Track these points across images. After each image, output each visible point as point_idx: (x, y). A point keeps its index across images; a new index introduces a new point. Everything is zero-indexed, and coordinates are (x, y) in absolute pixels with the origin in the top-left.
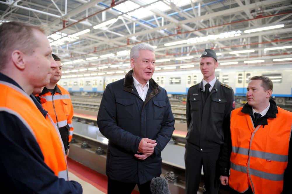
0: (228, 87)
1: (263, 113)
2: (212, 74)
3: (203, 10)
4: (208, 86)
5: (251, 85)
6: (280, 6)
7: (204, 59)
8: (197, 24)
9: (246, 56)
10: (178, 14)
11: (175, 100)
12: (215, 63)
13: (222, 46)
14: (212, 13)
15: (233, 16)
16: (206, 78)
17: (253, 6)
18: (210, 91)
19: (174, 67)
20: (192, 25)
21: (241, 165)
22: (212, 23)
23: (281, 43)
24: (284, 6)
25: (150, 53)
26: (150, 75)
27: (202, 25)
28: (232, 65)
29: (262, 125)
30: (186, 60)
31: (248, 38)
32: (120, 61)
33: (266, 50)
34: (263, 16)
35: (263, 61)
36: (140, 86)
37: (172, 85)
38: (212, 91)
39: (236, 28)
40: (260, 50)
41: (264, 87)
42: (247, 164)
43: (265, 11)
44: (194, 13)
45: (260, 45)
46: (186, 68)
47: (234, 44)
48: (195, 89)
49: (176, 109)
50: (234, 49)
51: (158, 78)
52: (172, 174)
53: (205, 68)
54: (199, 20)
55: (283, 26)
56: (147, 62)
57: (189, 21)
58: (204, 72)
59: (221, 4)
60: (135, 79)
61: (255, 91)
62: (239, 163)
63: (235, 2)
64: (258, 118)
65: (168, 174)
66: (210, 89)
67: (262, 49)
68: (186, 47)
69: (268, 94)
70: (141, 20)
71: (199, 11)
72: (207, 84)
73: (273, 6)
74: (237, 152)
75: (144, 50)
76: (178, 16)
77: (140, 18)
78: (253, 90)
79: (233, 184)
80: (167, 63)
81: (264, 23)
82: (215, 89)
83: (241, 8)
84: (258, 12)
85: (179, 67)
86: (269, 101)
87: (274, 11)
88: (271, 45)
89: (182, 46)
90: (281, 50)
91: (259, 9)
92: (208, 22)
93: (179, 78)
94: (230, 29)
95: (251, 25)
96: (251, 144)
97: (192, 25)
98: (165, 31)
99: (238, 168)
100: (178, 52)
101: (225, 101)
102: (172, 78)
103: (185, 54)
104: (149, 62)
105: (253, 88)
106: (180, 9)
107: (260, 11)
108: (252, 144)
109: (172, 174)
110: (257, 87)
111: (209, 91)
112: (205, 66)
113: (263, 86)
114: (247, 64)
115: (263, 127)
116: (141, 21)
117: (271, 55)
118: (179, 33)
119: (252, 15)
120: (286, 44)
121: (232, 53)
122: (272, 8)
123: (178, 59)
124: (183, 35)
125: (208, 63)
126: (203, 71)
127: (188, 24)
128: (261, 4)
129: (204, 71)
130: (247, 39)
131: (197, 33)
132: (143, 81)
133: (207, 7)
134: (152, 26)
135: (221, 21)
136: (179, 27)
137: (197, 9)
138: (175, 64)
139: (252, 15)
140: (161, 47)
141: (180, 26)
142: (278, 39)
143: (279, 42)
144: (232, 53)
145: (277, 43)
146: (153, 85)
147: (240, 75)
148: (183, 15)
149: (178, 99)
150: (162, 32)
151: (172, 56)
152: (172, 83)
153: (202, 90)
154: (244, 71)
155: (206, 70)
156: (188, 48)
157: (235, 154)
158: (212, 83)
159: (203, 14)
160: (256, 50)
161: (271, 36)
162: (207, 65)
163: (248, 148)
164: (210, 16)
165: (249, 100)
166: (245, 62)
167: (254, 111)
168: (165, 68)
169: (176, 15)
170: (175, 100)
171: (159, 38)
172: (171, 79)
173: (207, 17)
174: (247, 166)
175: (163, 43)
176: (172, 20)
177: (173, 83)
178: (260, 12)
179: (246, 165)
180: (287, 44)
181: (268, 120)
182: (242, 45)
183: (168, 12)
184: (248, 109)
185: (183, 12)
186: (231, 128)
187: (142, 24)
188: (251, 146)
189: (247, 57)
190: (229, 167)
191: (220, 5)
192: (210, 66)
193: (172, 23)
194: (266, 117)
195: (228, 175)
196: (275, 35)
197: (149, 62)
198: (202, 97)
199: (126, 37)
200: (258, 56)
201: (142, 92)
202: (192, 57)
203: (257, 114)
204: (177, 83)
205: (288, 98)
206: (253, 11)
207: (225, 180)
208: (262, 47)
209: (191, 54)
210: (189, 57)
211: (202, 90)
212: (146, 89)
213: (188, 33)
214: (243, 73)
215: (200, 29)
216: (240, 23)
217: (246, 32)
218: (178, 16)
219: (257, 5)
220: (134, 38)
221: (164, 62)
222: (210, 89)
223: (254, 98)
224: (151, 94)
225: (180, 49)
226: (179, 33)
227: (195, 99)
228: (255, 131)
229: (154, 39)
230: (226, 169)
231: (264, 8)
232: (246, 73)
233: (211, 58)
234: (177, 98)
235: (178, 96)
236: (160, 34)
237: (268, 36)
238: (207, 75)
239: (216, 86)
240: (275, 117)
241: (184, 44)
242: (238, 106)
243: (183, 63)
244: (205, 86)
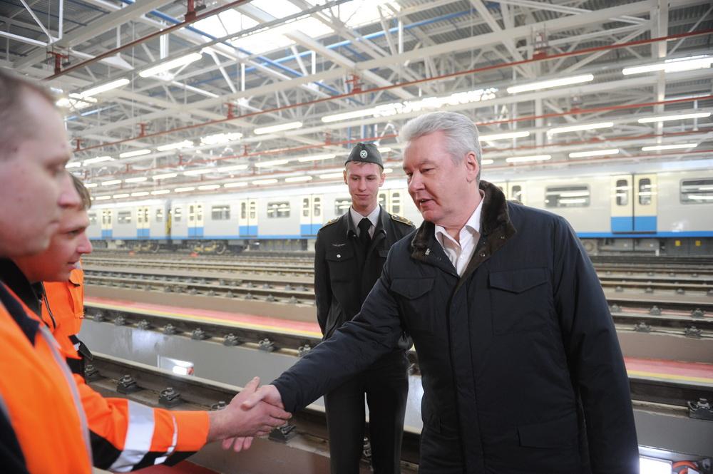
23: (583, 115)
30: (590, 114)
55: (590, 77)
90: (584, 132)
120: (593, 120)
147: (622, 183)
154: (507, 182)
180: (595, 117)
205: (605, 241)
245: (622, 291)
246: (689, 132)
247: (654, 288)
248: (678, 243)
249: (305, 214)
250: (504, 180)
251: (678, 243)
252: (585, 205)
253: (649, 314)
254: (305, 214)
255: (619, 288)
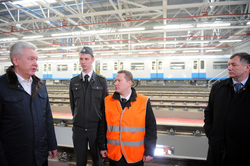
0: (103, 77)
1: (128, 98)
2: (90, 67)
3: (86, 8)
4: (87, 77)
5: (117, 78)
6: (142, 13)
7: (83, 55)
8: (81, 19)
9: (119, 48)
10: (63, 7)
11: (63, 85)
12: (92, 59)
13: (102, 40)
14: (93, 12)
15: (109, 15)
16: (84, 70)
17: (124, 11)
18: (89, 81)
19: (60, 55)
20: (76, 20)
21: (115, 140)
22: (93, 20)
24: (145, 13)
25: (32, 51)
26: (34, 71)
27: (84, 20)
28: (110, 56)
29: (127, 107)
31: (121, 35)
32: (3, 48)
33: (134, 45)
34: (131, 20)
35: (132, 53)
36: (25, 82)
37: (59, 72)
38: (90, 81)
39: (112, 26)
40: (129, 45)
41: (126, 79)
42: (119, 138)
43: (132, 15)
44: (78, 9)
45: (129, 41)
46: (72, 57)
47: (111, 39)
48: (76, 80)
49: (64, 93)
50: (111, 42)
51: (45, 65)
52: (65, 154)
53: (84, 63)
54: (82, 16)
55: (144, 29)
56: (32, 59)
57: (74, 16)
58: (83, 66)
59: (101, 5)
60: (18, 76)
61: (120, 82)
62: (114, 139)
63: (111, 5)
64: (124, 102)
65: (61, 155)
66: (89, 79)
67: (131, 44)
68: (72, 39)
69: (129, 84)
70: (26, 8)
71: (82, 8)
72: (86, 75)
73: (137, 12)
74: (112, 130)
75: (30, 48)
76: (64, 10)
77: (24, 6)
78: (119, 81)
79: (110, 155)
80: (54, 52)
81: (131, 26)
82: (93, 79)
83: (116, 11)
84: (128, 17)
85: (65, 55)
86: (131, 88)
87: (138, 16)
88: (137, 42)
89: (68, 37)
91: (128, 14)
92: (89, 18)
93: (66, 65)
94: (107, 27)
95: (123, 25)
96: (121, 122)
97: (76, 20)
98: (51, 22)
99: (113, 143)
100: (64, 42)
101: (101, 88)
102: (59, 66)
103: (70, 44)
104: (34, 59)
105: (119, 79)
106: (65, 4)
107: (129, 15)
108: (121, 122)
109: (65, 154)
110: (121, 79)
111: (88, 81)
112: (84, 61)
113: (125, 78)
114: (120, 55)
115: (128, 109)
116: (25, 9)
117: (137, 49)
118: (64, 25)
119: (124, 17)
121: (110, 46)
122: (137, 14)
123: (64, 48)
124: (68, 28)
125: (86, 59)
126: (82, 65)
127: (72, 19)
128: (130, 10)
129: (83, 65)
130: (120, 35)
131: (81, 27)
132: (27, 76)
133: (88, 5)
134: (37, 15)
135: (100, 19)
136: (64, 21)
137: (80, 6)
138: (61, 52)
139: (124, 17)
140: (47, 37)
141: (66, 19)
142: (141, 38)
143: (142, 40)
144: (110, 46)
145: (141, 41)
146: (36, 80)
148: (68, 9)
149: (66, 84)
150: (48, 22)
151: (59, 46)
152: (59, 70)
153: (83, 81)
155: (85, 65)
156: (73, 39)
157: (110, 132)
158: (90, 74)
159: (85, 11)
160: (127, 45)
161: (136, 34)
162: (85, 60)
163: (119, 125)
164: (92, 14)
165: (117, 89)
166: (119, 54)
167: (122, 97)
168: (52, 55)
169: (61, 8)
170: (63, 85)
171: (45, 28)
172: (58, 66)
173: (88, 14)
174: (119, 140)
175: (49, 33)
176: (57, 12)
177: (61, 70)
178: (129, 16)
179: (118, 139)
181: (131, 103)
182: (116, 41)
183: (54, 5)
184: (117, 96)
185: (67, 7)
186: (106, 111)
187: (26, 12)
188: (121, 124)
189: (120, 50)
190: (106, 142)
191: (99, 6)
192: (88, 61)
193: (57, 16)
194: (130, 101)
195: (107, 149)
196: (139, 35)
197: (34, 59)
198: (83, 87)
199: (10, 23)
200: (128, 50)
201: (27, 87)
202: (77, 47)
203: (124, 99)
204: (64, 70)
206: (124, 14)
207: (105, 153)
208: (130, 43)
209: (76, 45)
210: (74, 47)
211: (83, 81)
212: (30, 84)
213: (73, 26)
214: (118, 62)
215: (83, 24)
216: (114, 22)
217: (119, 30)
218: (64, 10)
219: (127, 11)
220: (18, 26)
221: (51, 50)
222: (89, 79)
223: (119, 88)
224: (36, 88)
225: (66, 39)
226: (64, 25)
227: (76, 89)
228: (123, 113)
229: (40, 29)
230: (104, 144)
231: (131, 14)
232: (120, 62)
233: (89, 55)
234: (64, 84)
235: (65, 82)
236: (46, 24)
237: (134, 34)
238: (85, 68)
239: (93, 77)
240: (136, 101)
241: (69, 35)
242: (111, 92)
243: (69, 52)
244: (85, 77)
245: (161, 97)
246: (174, 48)
247: (162, 95)
248: (169, 82)
249: (45, 70)
250: (118, 60)
251: (169, 82)
252: (143, 69)
253: (172, 104)
254: (45, 70)
255: (178, 96)
